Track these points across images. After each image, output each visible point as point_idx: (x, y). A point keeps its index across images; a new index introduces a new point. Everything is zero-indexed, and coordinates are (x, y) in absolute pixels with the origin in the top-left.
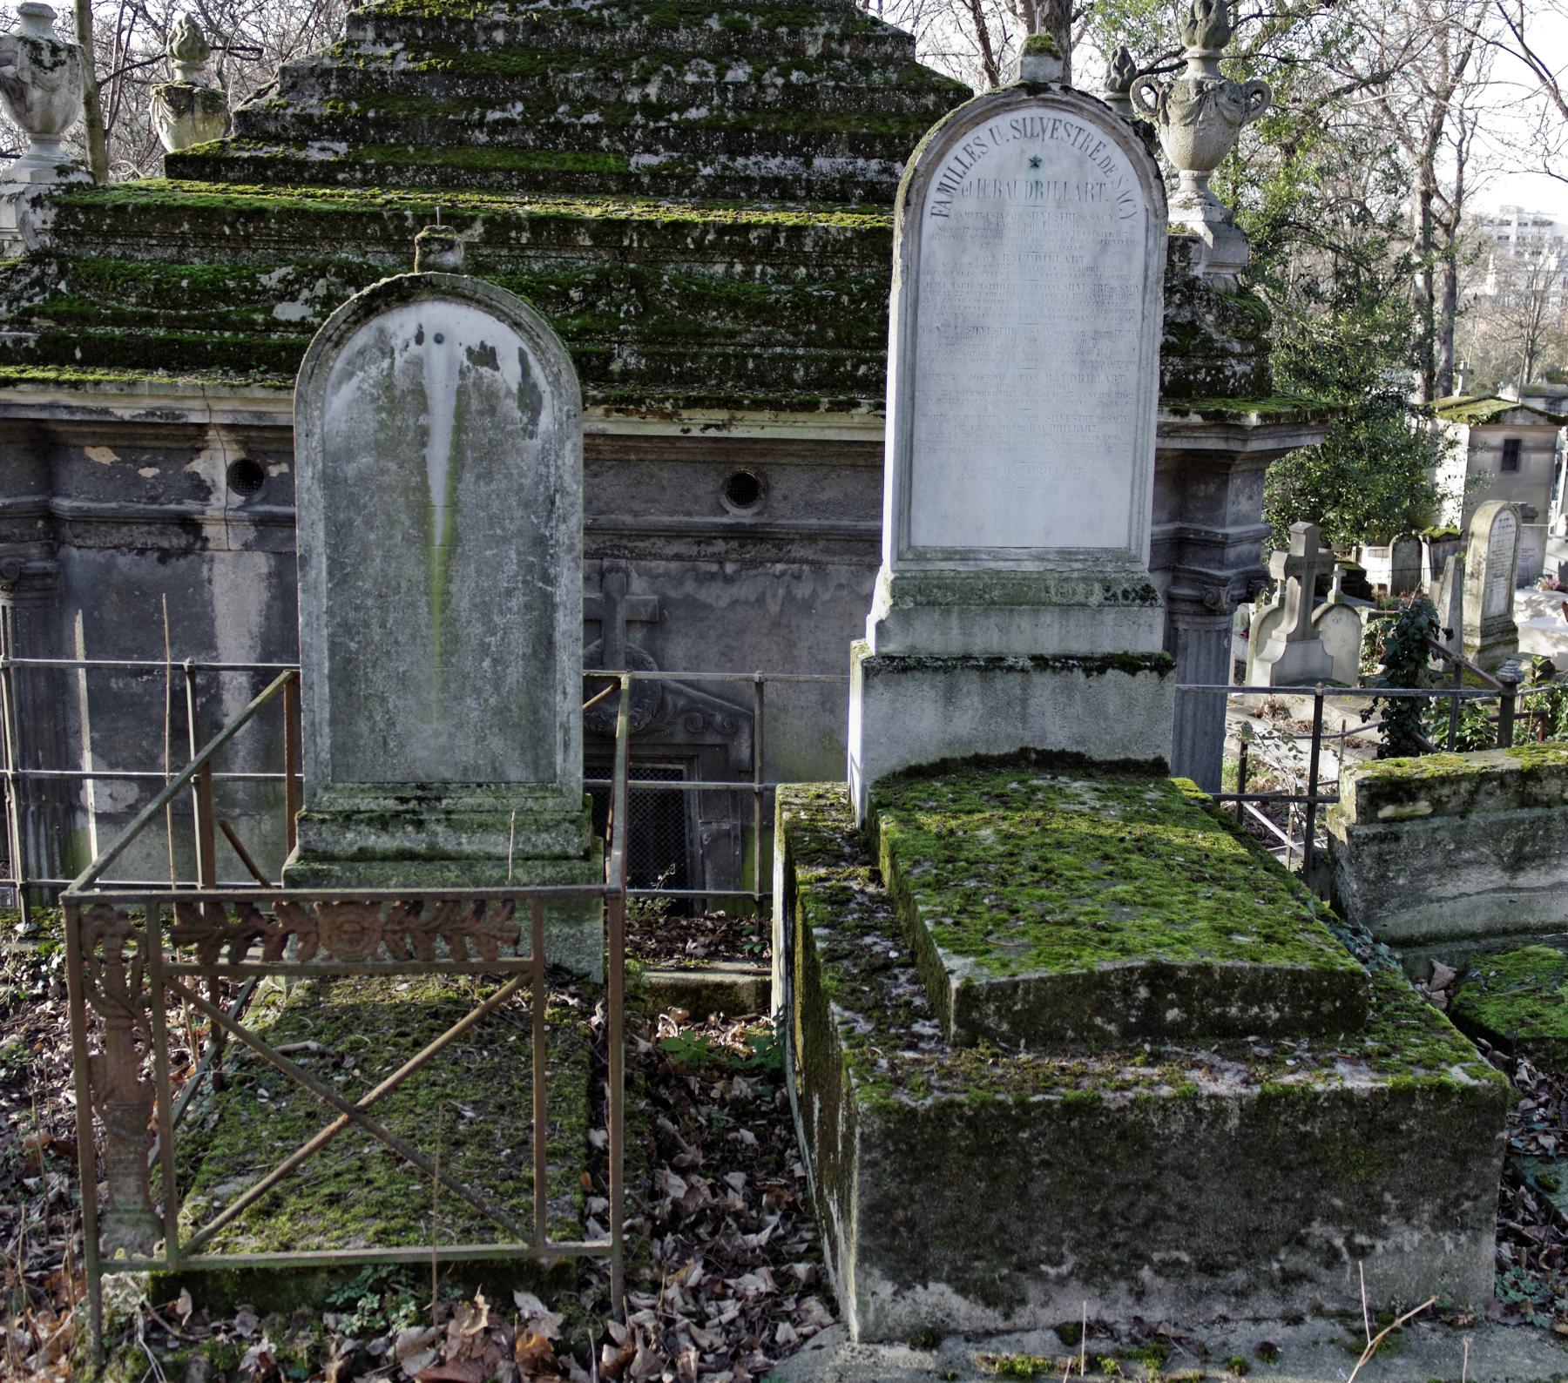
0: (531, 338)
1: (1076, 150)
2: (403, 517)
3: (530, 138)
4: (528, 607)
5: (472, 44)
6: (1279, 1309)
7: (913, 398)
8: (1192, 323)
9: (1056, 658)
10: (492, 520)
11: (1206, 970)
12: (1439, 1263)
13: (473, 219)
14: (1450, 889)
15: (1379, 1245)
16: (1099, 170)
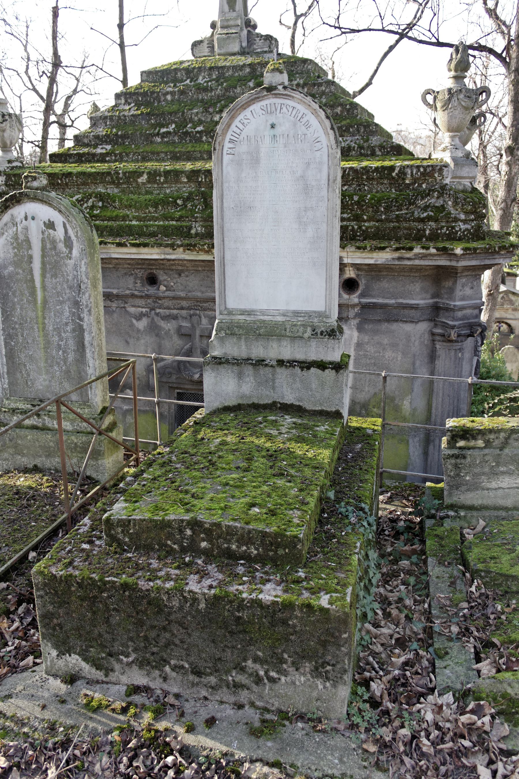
0: (67, 217)
1: (292, 118)
2: (26, 292)
3: (176, 139)
4: (74, 330)
5: (159, 102)
6: (232, 699)
7: (223, 241)
8: (443, 206)
9: (288, 362)
10: (58, 294)
11: (218, 525)
12: (315, 694)
13: (143, 172)
14: (494, 485)
15: (283, 679)
16: (303, 128)
